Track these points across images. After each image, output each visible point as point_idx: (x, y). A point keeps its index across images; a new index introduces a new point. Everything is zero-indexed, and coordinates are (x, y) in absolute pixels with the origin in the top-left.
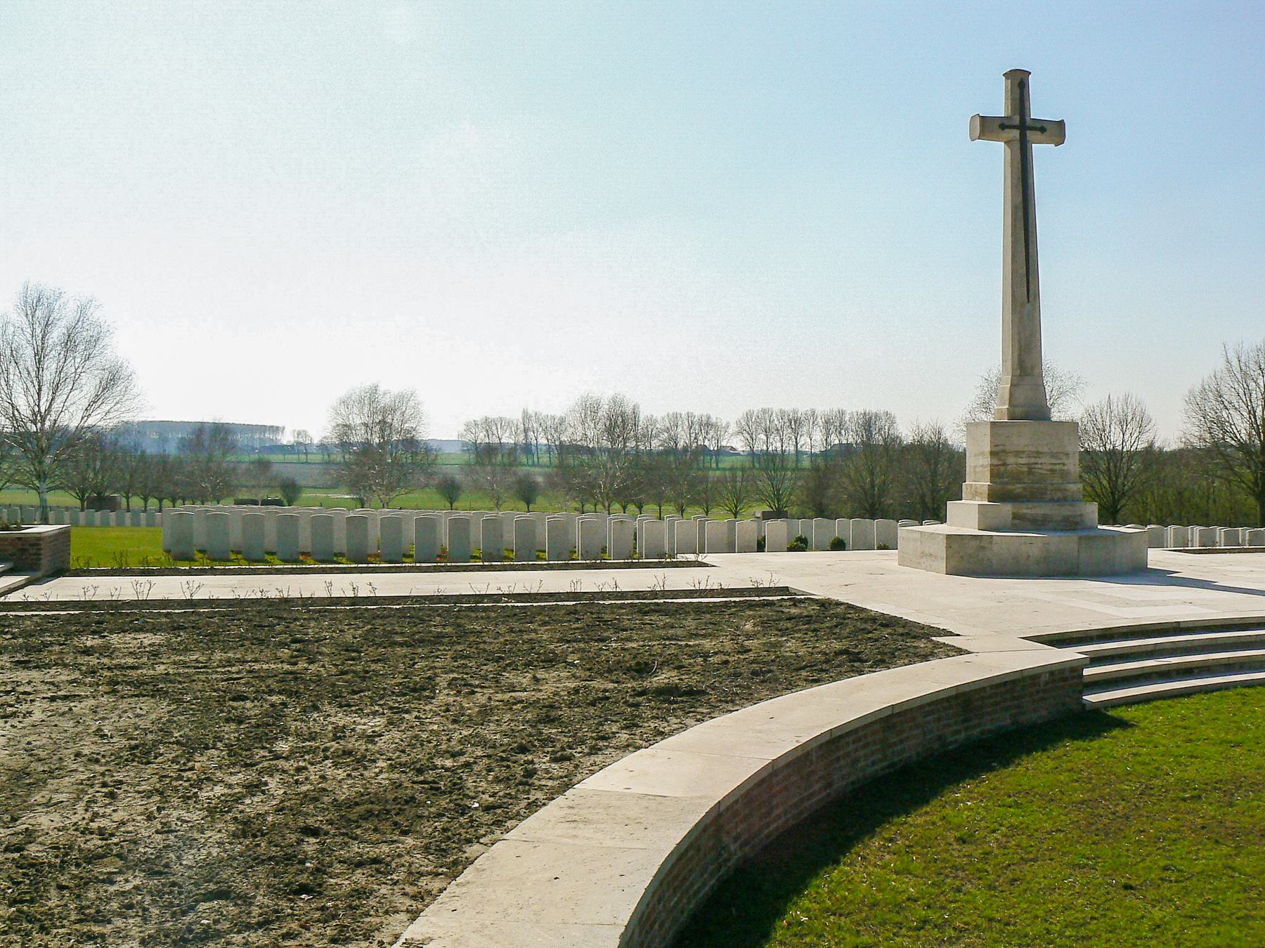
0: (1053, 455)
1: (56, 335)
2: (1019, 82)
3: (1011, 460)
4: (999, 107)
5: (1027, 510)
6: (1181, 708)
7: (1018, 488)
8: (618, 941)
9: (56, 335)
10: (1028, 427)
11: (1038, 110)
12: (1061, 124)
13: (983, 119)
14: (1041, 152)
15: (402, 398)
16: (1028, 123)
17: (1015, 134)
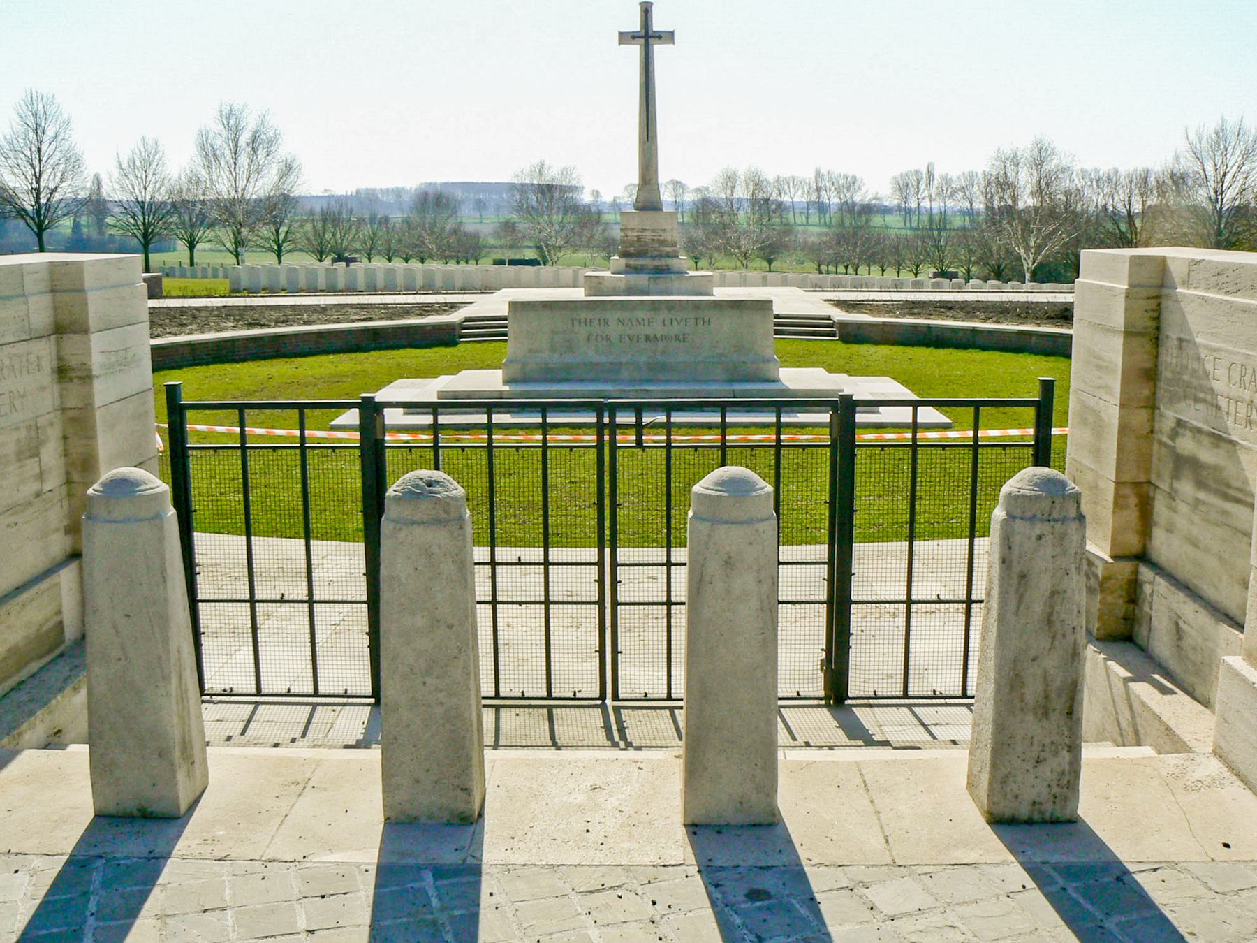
0: (653, 231)
1: (244, 138)
2: (646, 11)
3: (630, 233)
4: (636, 26)
5: (632, 262)
7: (632, 250)
8: (364, 579)
9: (244, 138)
11: (657, 25)
13: (621, 34)
14: (658, 49)
15: (565, 172)
16: (650, 33)
17: (643, 41)
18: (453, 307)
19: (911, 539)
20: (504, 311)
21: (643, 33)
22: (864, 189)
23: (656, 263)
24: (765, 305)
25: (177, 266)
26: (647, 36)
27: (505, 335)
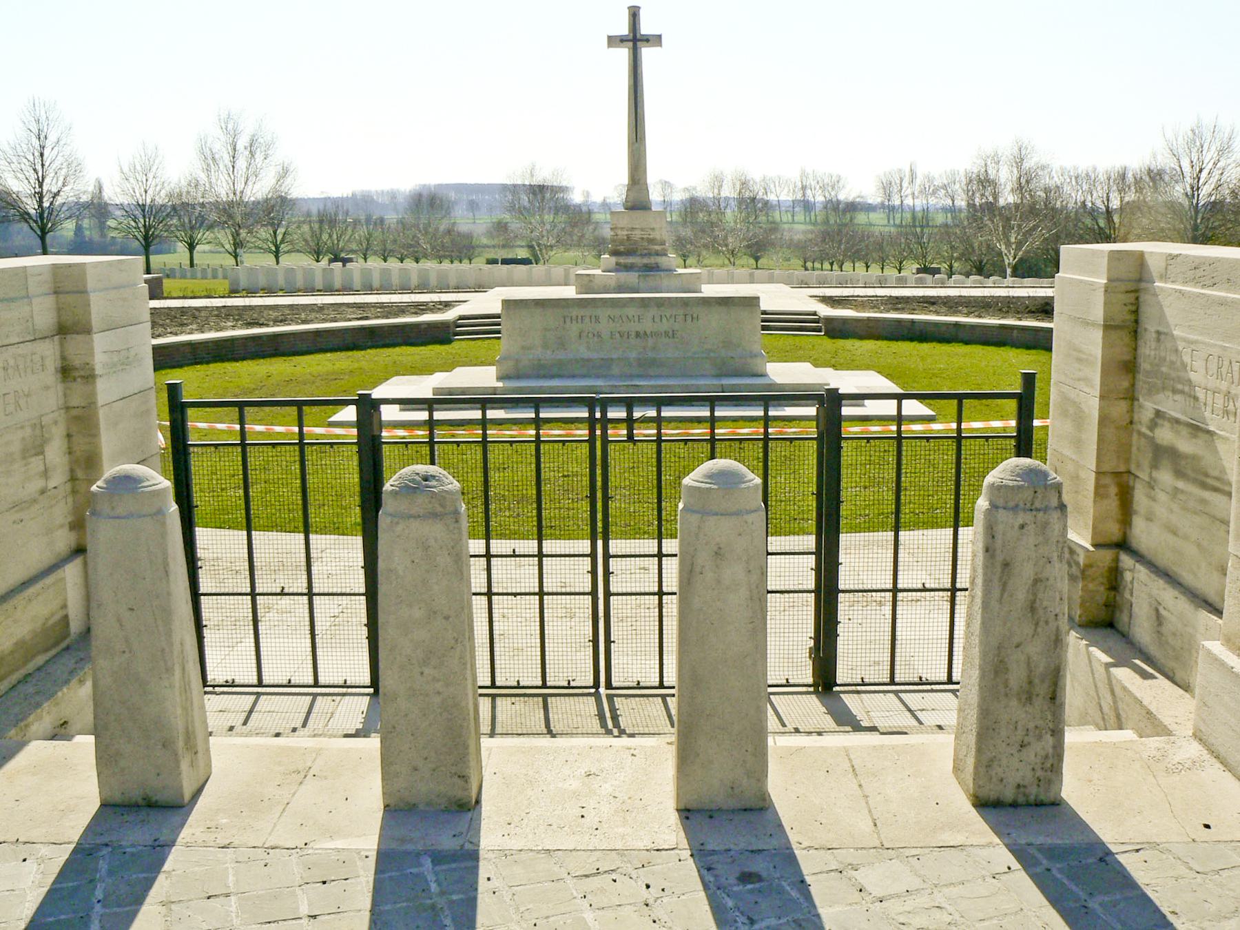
0: (642, 230)
2: (634, 14)
3: (619, 232)
4: (624, 30)
6: (487, 342)
7: (622, 248)
10: (638, 214)
11: (645, 29)
12: (660, 36)
13: (610, 38)
14: (647, 53)
17: (631, 44)
20: (496, 309)
26: (635, 40)
27: (499, 332)
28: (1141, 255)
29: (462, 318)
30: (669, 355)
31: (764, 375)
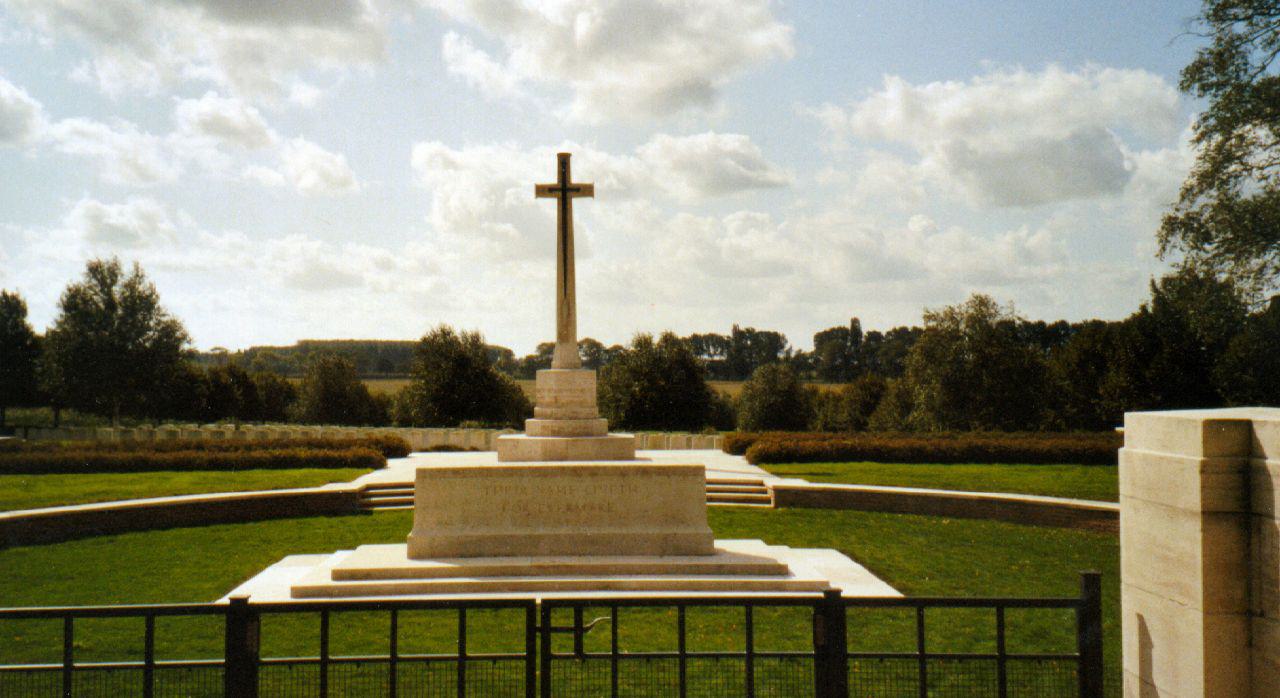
2: (564, 161)
4: (552, 179)
11: (576, 177)
14: (577, 203)
17: (560, 194)
18: (649, 460)
19: (394, 660)
20: (411, 478)
21: (560, 186)
22: (787, 347)
23: (213, 456)
24: (699, 471)
25: (1179, 255)
26: (565, 191)
27: (411, 503)
28: (1248, 425)
29: (369, 487)
30: (232, 426)
31: (713, 553)
